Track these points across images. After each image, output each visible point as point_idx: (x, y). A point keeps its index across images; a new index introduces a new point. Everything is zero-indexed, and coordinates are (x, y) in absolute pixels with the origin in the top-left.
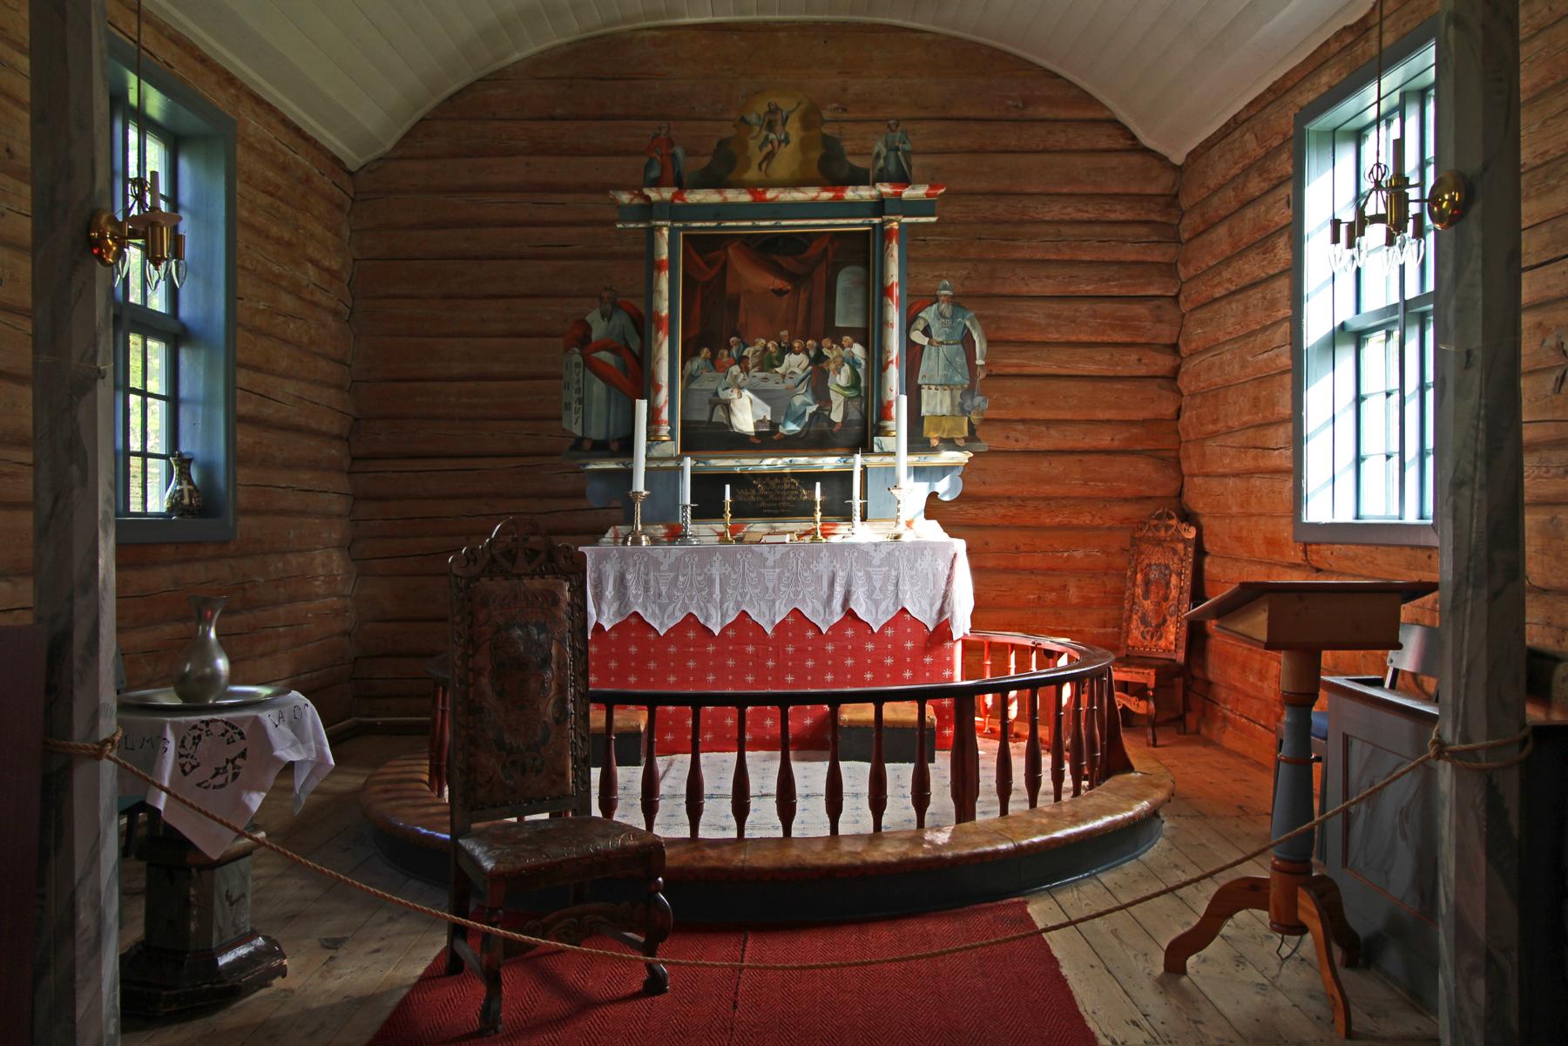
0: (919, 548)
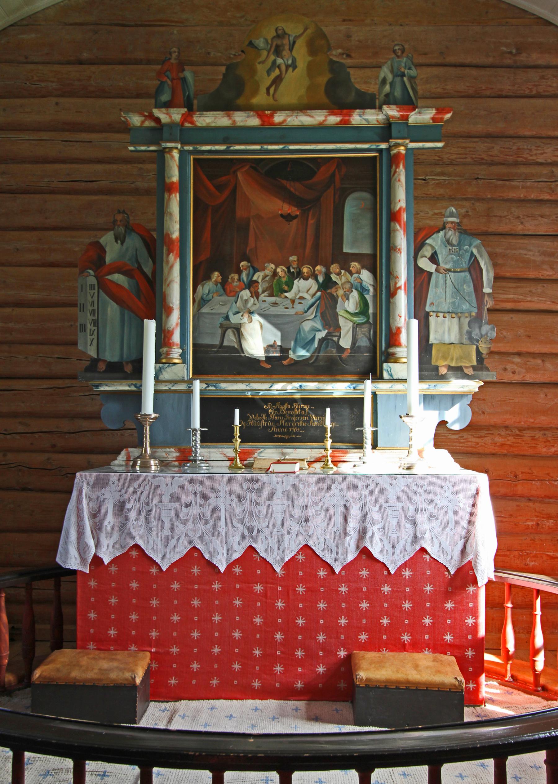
0: (436, 484)
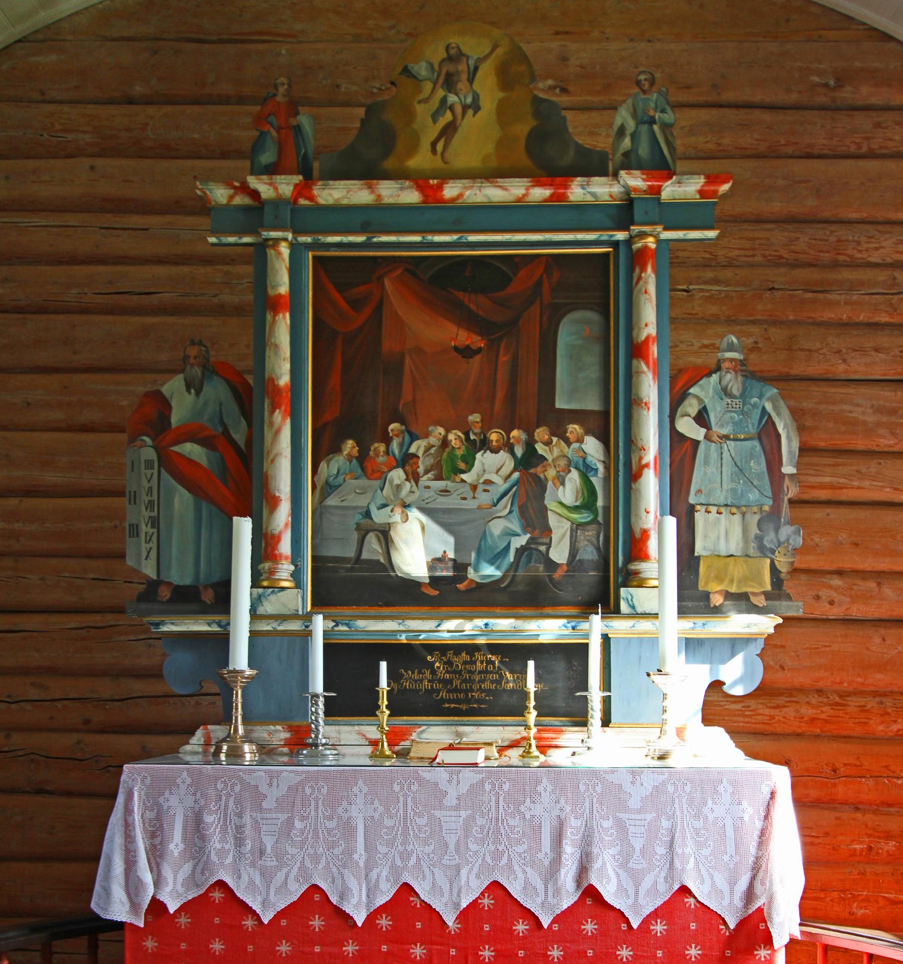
0: (706, 782)
